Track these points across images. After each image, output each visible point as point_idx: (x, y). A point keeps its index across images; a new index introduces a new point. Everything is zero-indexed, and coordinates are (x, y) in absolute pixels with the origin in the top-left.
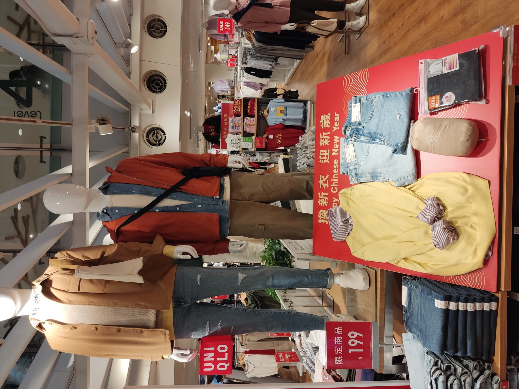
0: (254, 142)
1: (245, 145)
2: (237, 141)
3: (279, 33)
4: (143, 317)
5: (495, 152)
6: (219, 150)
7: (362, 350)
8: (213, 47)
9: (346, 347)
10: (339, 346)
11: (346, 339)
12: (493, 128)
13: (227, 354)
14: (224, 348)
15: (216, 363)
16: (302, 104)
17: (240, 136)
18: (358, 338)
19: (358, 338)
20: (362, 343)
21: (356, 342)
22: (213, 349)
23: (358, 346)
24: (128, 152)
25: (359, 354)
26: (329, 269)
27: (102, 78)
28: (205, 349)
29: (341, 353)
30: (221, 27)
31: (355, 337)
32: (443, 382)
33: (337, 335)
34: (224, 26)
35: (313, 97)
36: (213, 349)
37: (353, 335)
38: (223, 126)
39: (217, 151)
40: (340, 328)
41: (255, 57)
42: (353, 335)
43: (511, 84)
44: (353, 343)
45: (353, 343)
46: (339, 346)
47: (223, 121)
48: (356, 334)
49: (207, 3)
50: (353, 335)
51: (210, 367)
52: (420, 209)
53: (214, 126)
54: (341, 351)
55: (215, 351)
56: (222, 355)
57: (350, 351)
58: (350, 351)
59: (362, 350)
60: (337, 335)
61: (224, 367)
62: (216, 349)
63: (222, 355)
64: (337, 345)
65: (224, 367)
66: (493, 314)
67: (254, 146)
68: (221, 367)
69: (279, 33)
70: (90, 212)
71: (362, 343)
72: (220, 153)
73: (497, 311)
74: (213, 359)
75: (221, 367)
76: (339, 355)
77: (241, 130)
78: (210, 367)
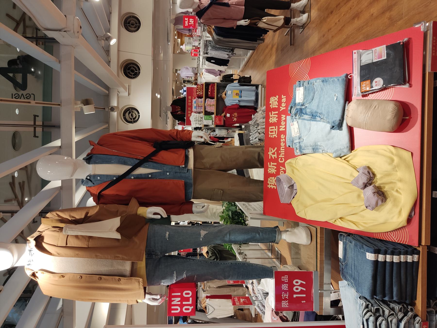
0: (214, 120)
1: (206, 122)
2: (200, 119)
3: (235, 28)
4: (120, 268)
5: (417, 128)
6: (184, 127)
7: (305, 295)
8: (179, 40)
9: (292, 292)
10: (285, 292)
11: (291, 286)
13: (191, 299)
14: (188, 294)
15: (181, 306)
16: (254, 88)
17: (202, 115)
18: (301, 285)
19: (301, 285)
20: (305, 289)
21: (300, 288)
22: (179, 294)
23: (302, 292)
24: (108, 128)
25: (302, 298)
27: (86, 66)
28: (173, 294)
29: (287, 297)
31: (299, 284)
32: (373, 322)
33: (284, 283)
34: (189, 22)
35: (263, 82)
36: (179, 294)
37: (297, 282)
38: (188, 106)
39: (183, 127)
40: (286, 277)
42: (297, 282)
43: (430, 71)
44: (297, 289)
45: (297, 289)
46: (285, 292)
47: (188, 102)
48: (300, 282)
49: (174, 3)
50: (297, 282)
51: (177, 309)
52: (353, 176)
53: (180, 106)
54: (287, 296)
55: (181, 296)
56: (187, 299)
57: (295, 296)
58: (295, 296)
59: (305, 295)
60: (284, 283)
61: (188, 309)
62: (182, 294)
63: (187, 299)
64: (284, 291)
65: (188, 309)
66: (415, 265)
67: (213, 123)
68: (186, 309)
69: (235, 28)
70: (76, 179)
71: (305, 289)
72: (185, 129)
74: (179, 303)
75: (186, 309)
76: (285, 299)
77: (203, 110)
78: (177, 309)
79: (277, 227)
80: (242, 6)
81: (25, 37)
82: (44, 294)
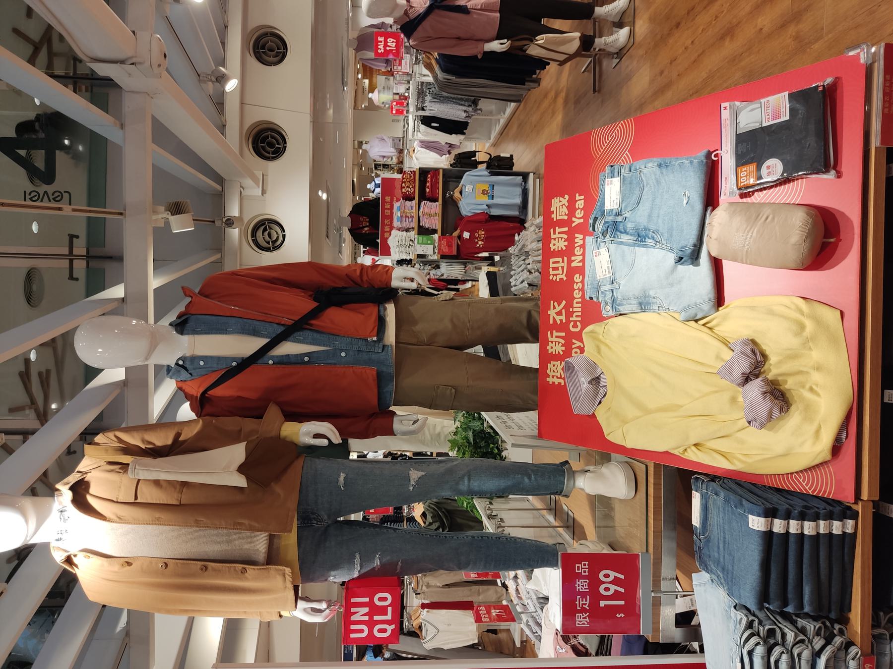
0: (437, 245)
1: (421, 249)
2: (408, 243)
3: (480, 57)
4: (246, 546)
5: (851, 261)
6: (376, 258)
7: (622, 603)
8: (367, 81)
9: (596, 596)
10: (583, 595)
11: (595, 583)
12: (848, 219)
13: (390, 609)
14: (385, 599)
15: (371, 624)
16: (519, 179)
17: (413, 234)
18: (616, 582)
19: (616, 582)
20: (622, 590)
21: (613, 588)
22: (366, 600)
23: (616, 596)
25: (618, 608)
26: (567, 462)
28: (354, 600)
29: (586, 607)
30: (381, 47)
31: (611, 579)
32: (763, 658)
33: (580, 576)
34: (386, 45)
35: (538, 166)
36: (366, 600)
37: (607, 576)
38: (385, 217)
39: (373, 259)
40: (585, 565)
41: (438, 99)
42: (607, 576)
43: (879, 144)
44: (607, 589)
45: (607, 589)
46: (583, 595)
47: (384, 209)
49: (356, 6)
50: (608, 575)
51: (362, 631)
52: (722, 360)
53: (368, 217)
54: (586, 603)
55: (371, 604)
56: (383, 611)
57: (602, 604)
58: (602, 604)
59: (622, 603)
60: (580, 576)
61: (385, 631)
62: (372, 600)
63: (383, 611)
64: (580, 593)
65: (385, 631)
66: (848, 540)
67: (436, 251)
68: (380, 631)
69: (480, 57)
70: (155, 365)
71: (622, 590)
72: (378, 263)
74: (367, 618)
75: (380, 631)
76: (583, 610)
77: (414, 224)
78: (362, 631)
80: (495, 11)
81: (51, 76)
82: (91, 599)
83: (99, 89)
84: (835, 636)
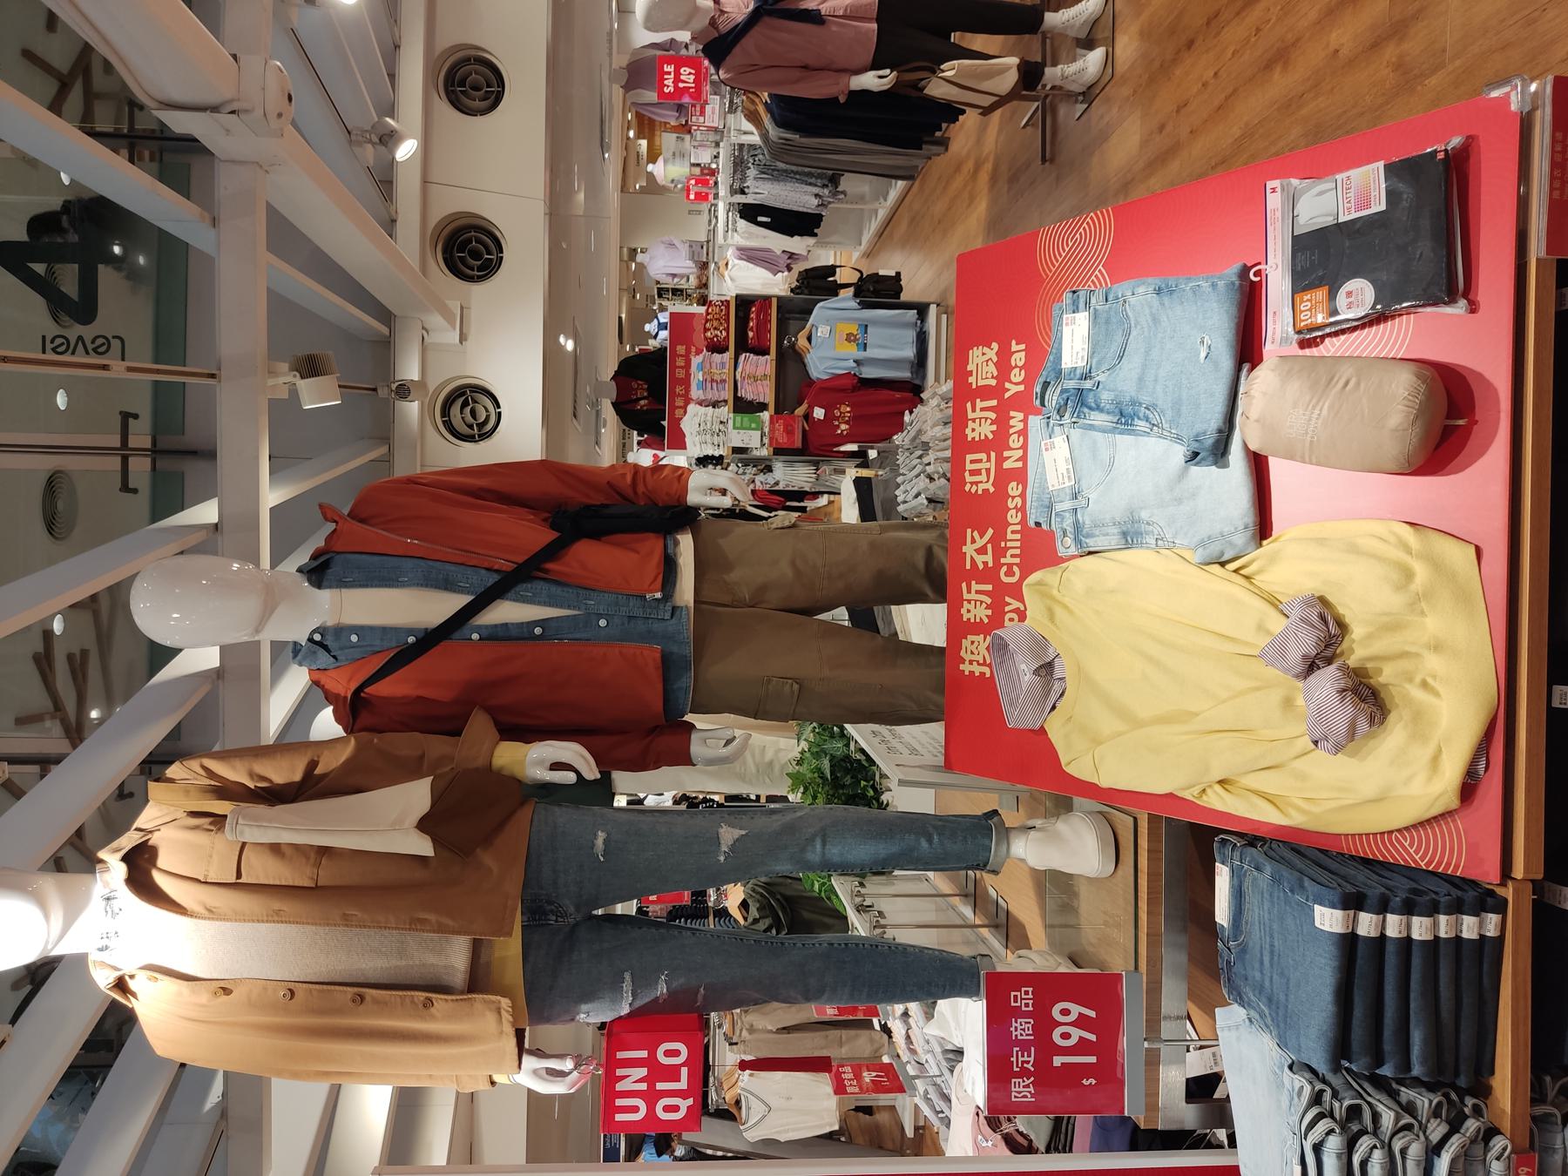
0: (766, 430)
1: (739, 437)
2: (716, 427)
3: (842, 100)
4: (431, 959)
5: (1495, 459)
6: (661, 454)
7: (1093, 1059)
8: (644, 143)
9: (1046, 1048)
10: (1024, 1046)
11: (1044, 1025)
12: (1488, 386)
13: (684, 1071)
14: (676, 1053)
15: (651, 1097)
16: (912, 314)
17: (725, 412)
18: (1081, 1022)
19: (1081, 1022)
20: (1093, 1037)
21: (1076, 1034)
22: (643, 1054)
23: (1082, 1047)
25: (1085, 1070)
27: (309, 235)
28: (621, 1055)
29: (1029, 1066)
31: (1072, 1017)
32: (1339, 1156)
33: (1018, 1013)
34: (677, 80)
35: (945, 293)
36: (643, 1054)
37: (1065, 1012)
38: (675, 381)
39: (655, 456)
40: (1027, 993)
41: (769, 173)
42: (1065, 1012)
44: (1066, 1036)
45: (1066, 1036)
46: (1024, 1046)
47: (674, 367)
49: (625, 10)
50: (1067, 1012)
51: (635, 1109)
52: (1268, 632)
53: (646, 382)
54: (1029, 1060)
55: (651, 1062)
56: (672, 1073)
57: (1058, 1061)
58: (1058, 1061)
59: (1093, 1059)
60: (1018, 1013)
61: (676, 1109)
62: (653, 1054)
63: (672, 1073)
64: (1018, 1043)
65: (676, 1109)
66: (1488, 949)
67: (766, 441)
68: (667, 1109)
69: (842, 100)
71: (1093, 1037)
72: (663, 462)
73: (1500, 940)
74: (644, 1086)
75: (667, 1109)
76: (1024, 1073)
77: (727, 394)
78: (635, 1109)
79: (995, 812)
80: (869, 20)
81: (89, 134)
83: (174, 156)
84: (1466, 1117)
